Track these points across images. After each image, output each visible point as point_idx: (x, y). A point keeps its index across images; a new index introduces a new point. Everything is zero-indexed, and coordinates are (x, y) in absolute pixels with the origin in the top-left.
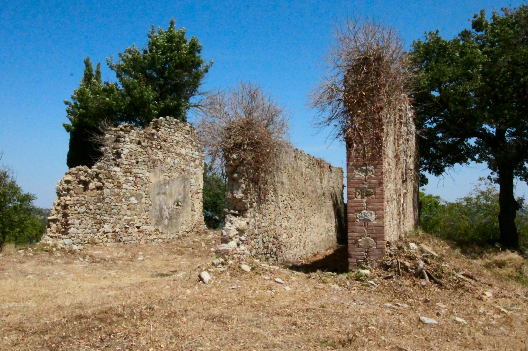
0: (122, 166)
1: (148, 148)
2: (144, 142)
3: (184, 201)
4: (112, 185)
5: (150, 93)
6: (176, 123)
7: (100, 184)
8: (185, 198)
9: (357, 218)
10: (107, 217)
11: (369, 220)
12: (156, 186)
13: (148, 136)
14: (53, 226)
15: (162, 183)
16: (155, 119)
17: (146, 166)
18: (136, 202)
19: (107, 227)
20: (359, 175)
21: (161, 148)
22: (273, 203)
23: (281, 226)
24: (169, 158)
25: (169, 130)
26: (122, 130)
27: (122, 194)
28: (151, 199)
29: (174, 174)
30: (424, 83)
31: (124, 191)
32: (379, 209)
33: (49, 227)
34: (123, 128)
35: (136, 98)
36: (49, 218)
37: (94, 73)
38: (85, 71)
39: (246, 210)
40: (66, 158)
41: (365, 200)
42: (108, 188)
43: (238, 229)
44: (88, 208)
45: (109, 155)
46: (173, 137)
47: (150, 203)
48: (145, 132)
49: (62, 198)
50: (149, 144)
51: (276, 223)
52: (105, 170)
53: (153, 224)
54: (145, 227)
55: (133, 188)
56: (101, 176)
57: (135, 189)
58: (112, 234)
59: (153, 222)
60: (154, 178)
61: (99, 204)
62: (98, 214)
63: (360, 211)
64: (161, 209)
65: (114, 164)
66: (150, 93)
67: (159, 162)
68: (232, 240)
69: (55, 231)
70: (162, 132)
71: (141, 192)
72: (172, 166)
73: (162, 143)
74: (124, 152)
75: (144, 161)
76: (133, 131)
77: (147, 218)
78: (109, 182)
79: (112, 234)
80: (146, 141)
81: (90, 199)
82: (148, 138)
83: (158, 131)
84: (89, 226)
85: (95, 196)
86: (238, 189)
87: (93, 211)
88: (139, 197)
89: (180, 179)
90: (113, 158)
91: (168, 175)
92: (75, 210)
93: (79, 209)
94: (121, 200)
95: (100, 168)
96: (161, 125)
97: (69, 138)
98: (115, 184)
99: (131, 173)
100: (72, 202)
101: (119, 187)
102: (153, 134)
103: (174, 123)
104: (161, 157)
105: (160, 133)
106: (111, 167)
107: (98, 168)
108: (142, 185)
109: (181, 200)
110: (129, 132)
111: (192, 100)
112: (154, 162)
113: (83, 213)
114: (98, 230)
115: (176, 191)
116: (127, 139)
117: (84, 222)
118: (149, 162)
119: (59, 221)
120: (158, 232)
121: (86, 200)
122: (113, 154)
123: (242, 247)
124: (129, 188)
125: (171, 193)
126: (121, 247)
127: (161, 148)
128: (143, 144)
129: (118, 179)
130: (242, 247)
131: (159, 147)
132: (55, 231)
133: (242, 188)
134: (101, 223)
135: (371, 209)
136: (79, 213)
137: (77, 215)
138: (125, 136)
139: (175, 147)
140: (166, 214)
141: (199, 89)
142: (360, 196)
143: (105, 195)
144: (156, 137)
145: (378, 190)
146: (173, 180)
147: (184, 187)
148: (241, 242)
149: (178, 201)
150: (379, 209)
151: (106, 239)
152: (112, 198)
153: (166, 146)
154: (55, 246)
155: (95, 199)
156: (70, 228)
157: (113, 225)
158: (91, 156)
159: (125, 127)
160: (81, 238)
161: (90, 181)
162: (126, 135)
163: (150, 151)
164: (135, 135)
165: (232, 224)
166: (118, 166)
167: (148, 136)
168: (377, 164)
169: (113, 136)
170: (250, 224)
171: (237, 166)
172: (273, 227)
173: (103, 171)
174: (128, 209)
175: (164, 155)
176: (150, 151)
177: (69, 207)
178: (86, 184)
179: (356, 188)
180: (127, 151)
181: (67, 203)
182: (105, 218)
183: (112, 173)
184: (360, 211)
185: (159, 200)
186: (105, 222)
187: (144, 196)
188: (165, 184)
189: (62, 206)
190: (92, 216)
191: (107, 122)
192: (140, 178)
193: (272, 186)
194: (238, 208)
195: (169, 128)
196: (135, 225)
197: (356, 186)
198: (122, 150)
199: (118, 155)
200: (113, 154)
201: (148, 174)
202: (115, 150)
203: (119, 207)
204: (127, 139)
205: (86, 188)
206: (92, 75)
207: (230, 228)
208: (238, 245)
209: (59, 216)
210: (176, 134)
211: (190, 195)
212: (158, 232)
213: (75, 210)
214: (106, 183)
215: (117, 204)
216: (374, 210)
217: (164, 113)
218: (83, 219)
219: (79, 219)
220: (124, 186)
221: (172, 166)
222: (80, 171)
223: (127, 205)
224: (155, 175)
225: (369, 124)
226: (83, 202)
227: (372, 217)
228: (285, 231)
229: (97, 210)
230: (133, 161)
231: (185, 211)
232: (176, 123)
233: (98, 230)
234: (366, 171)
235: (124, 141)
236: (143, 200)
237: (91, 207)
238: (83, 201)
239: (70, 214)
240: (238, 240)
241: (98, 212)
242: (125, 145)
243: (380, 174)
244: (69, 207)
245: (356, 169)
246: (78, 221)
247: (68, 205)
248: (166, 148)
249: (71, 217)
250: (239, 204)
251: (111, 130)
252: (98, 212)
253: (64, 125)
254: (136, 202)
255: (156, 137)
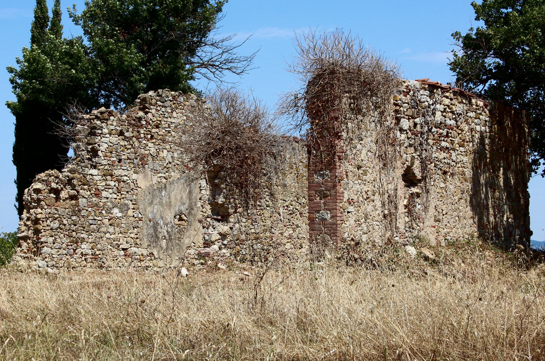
0: (100, 167)
1: (134, 139)
2: (128, 131)
3: (190, 213)
4: (89, 193)
5: (133, 56)
6: (174, 97)
7: (73, 192)
8: (191, 208)
9: (316, 218)
10: (84, 236)
11: (326, 219)
12: (147, 193)
13: (133, 122)
14: (24, 245)
15: (155, 188)
16: (142, 95)
17: (132, 166)
18: (120, 215)
19: (85, 248)
20: (317, 179)
21: (152, 137)
22: (268, 208)
23: (282, 234)
24: (165, 151)
25: (163, 109)
26: (97, 118)
27: (101, 204)
28: (141, 211)
29: (173, 174)
30: (496, 44)
31: (104, 200)
32: (333, 209)
33: (20, 246)
34: (99, 115)
35: (112, 65)
36: (19, 235)
37: (51, 15)
38: (36, 12)
39: (229, 215)
40: (11, 152)
41: (322, 201)
42: (83, 197)
43: (220, 234)
44: (61, 223)
45: (83, 153)
46: (169, 120)
47: (140, 216)
48: (128, 116)
49: (32, 211)
50: (135, 133)
51: (273, 230)
52: (80, 173)
53: (146, 244)
54: (134, 249)
55: (115, 196)
56: (75, 182)
57: (118, 197)
58: (91, 256)
59: (146, 243)
60: (144, 181)
61: (74, 218)
62: (73, 231)
63: (318, 212)
64: (155, 226)
65: (89, 166)
66: (133, 56)
67: (150, 158)
68: (214, 244)
69: (26, 251)
70: (153, 114)
71: (126, 202)
72: (170, 163)
73: (154, 130)
74: (102, 148)
75: (128, 159)
76: (112, 118)
77: (136, 236)
78: (84, 190)
79: (91, 256)
80: (131, 130)
81: (64, 212)
82: (134, 125)
83: (146, 113)
84: (64, 245)
85: (69, 208)
86: (219, 195)
87: (68, 227)
88: (124, 208)
89: (182, 181)
90: (88, 156)
91: (163, 175)
92: (48, 226)
93: (52, 224)
94: (101, 213)
95: (72, 171)
96: (151, 104)
97: (15, 122)
98: (92, 192)
99: (111, 175)
100: (43, 216)
101: (98, 195)
102: (140, 119)
103: (170, 98)
104: (153, 151)
105: (150, 115)
106: (87, 169)
107: (70, 171)
108: (127, 192)
109: (186, 212)
110: (107, 120)
111: (204, 53)
112: (143, 158)
113: (56, 229)
114: (75, 250)
115: (176, 199)
116: (105, 131)
117: (59, 240)
118: (137, 159)
119: (29, 238)
120: (153, 258)
121: (59, 213)
122: (88, 151)
123: (224, 251)
124: (110, 196)
125: (170, 202)
126: (104, 274)
127: (152, 137)
128: (127, 134)
129: (96, 184)
130: (224, 251)
131: (149, 136)
132: (26, 251)
133: (224, 193)
134: (77, 242)
135: (327, 210)
136: (52, 229)
137: (50, 231)
138: (102, 127)
139: (173, 133)
140: (163, 231)
141: (212, 36)
142: (319, 198)
143: (81, 206)
144: (144, 123)
145: (333, 192)
146: (171, 184)
147: (190, 192)
148: (223, 246)
149: (181, 214)
150: (333, 209)
151: (84, 262)
152: (90, 209)
153: (159, 133)
154: (29, 267)
155: (69, 212)
156: (43, 247)
157: (92, 245)
158: (59, 155)
159: (102, 113)
160: (55, 259)
161: (62, 189)
162: (104, 125)
163: (137, 144)
164: (115, 124)
165: (214, 228)
166: (95, 167)
167: (133, 122)
168: (332, 168)
169: (86, 127)
170: (234, 229)
171: (219, 171)
172: (268, 234)
173: (76, 175)
174: (111, 225)
175: (157, 147)
176: (137, 144)
177: (41, 222)
178: (57, 192)
179: (315, 191)
180: (106, 146)
181: (39, 216)
182: (82, 236)
183: (88, 177)
184: (318, 212)
185: (152, 212)
186: (83, 240)
187: (131, 206)
188: (160, 190)
189: (32, 221)
190: (67, 233)
191: (77, 108)
192: (124, 182)
193: (266, 190)
194: (221, 213)
195: (163, 106)
196: (121, 246)
197: (316, 189)
198: (99, 145)
199: (94, 153)
200: (88, 151)
201: (135, 176)
202: (90, 147)
203: (99, 222)
204: (105, 131)
205: (58, 199)
206: (46, 18)
207: (212, 233)
208: (220, 248)
209: (30, 233)
210: (174, 114)
211: (199, 204)
212: (153, 258)
213: (48, 226)
214: (81, 191)
215: (95, 218)
216: (330, 210)
217: (155, 84)
218: (57, 237)
219: (52, 236)
220: (104, 194)
221: (170, 163)
222: (50, 176)
223: (109, 220)
224: (145, 176)
225: (325, 133)
226: (56, 216)
227: (328, 216)
228: (289, 240)
229: (72, 226)
230: (115, 159)
231: (192, 228)
232: (174, 97)
233: (75, 250)
234: (322, 176)
235: (102, 133)
236: (130, 213)
237: (65, 222)
238: (55, 214)
239: (43, 231)
240: (220, 244)
241: (74, 228)
242: (103, 139)
243: (334, 177)
244: (41, 222)
245: (316, 173)
246: (51, 240)
247: (39, 219)
248: (159, 137)
249: (44, 233)
250: (222, 209)
251: (83, 118)
252: (74, 228)
253: (9, 105)
254: (120, 215)
255: (144, 123)
